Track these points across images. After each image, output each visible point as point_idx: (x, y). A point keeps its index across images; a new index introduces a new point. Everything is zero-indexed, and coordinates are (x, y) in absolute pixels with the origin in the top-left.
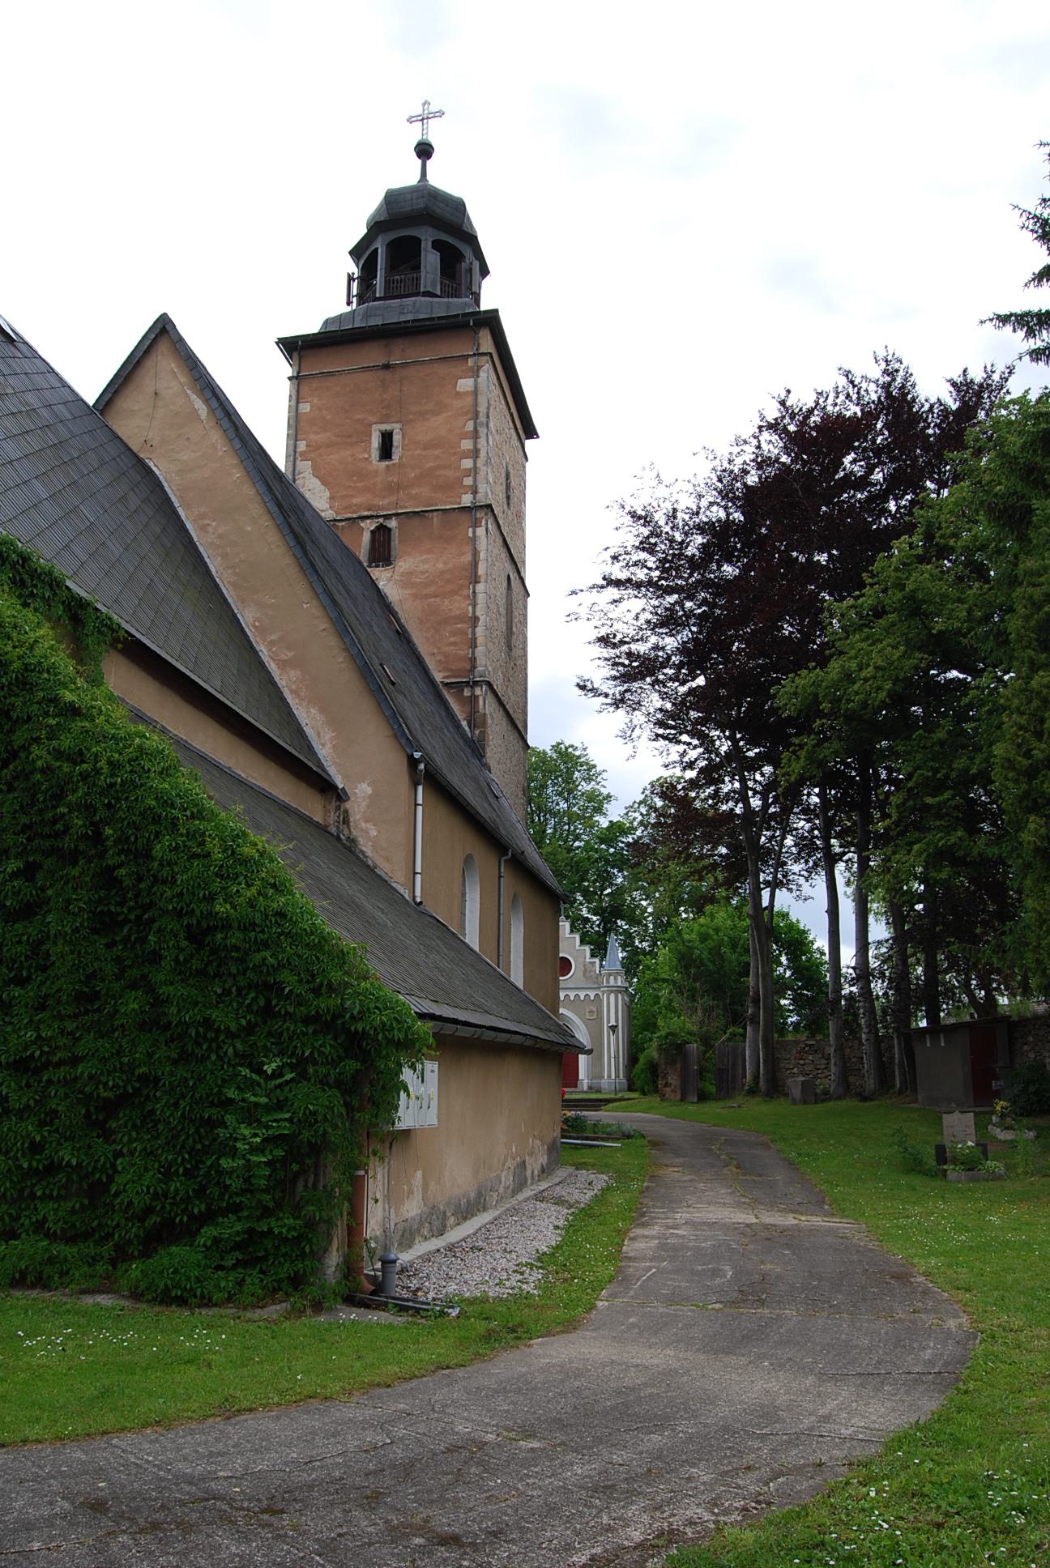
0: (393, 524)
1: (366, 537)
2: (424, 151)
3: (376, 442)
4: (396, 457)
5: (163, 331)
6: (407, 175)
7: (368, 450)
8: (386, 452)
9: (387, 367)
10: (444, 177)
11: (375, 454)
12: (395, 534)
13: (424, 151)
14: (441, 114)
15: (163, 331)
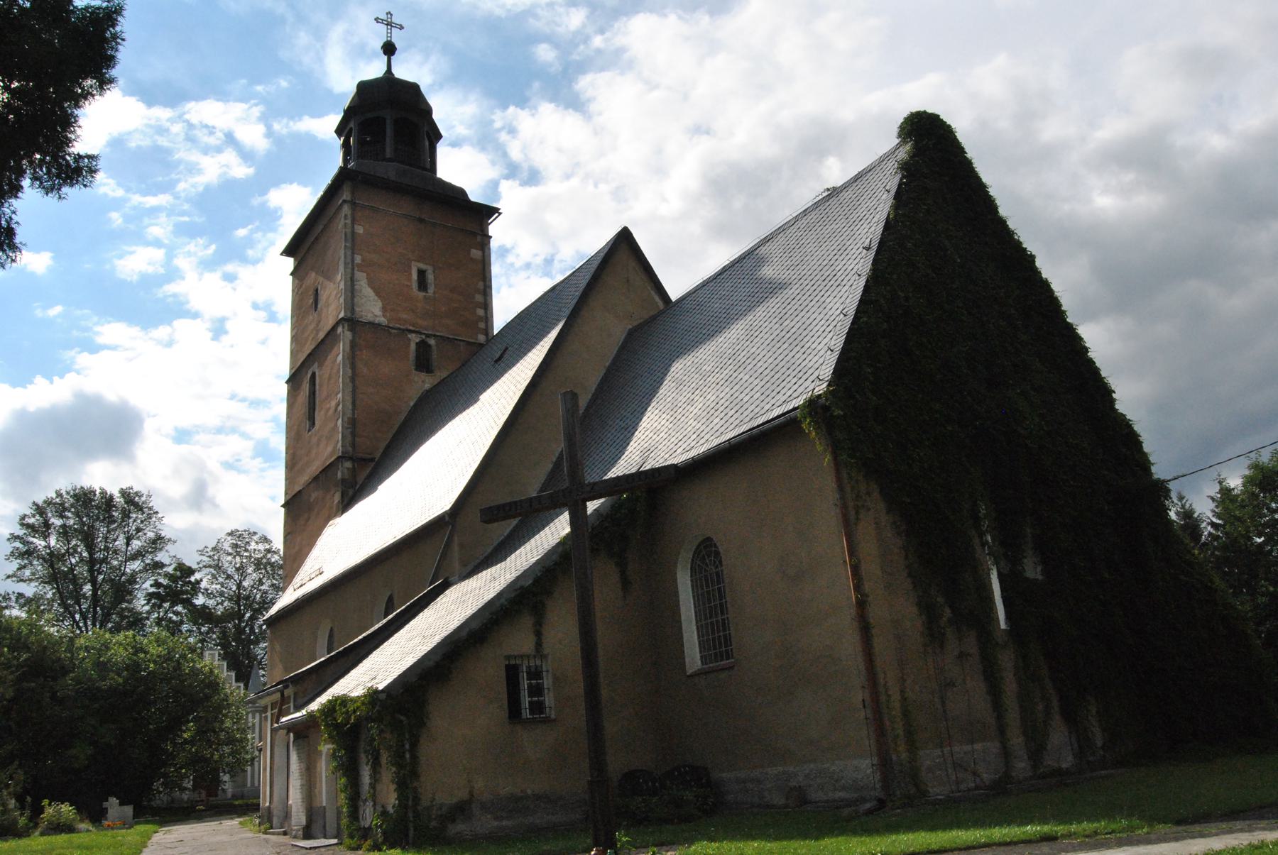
0: (432, 342)
1: (413, 347)
2: (389, 49)
3: (415, 276)
4: (431, 290)
5: (625, 240)
6: (375, 70)
7: (410, 279)
8: (422, 284)
9: (421, 220)
10: (402, 72)
11: (415, 285)
12: (434, 348)
13: (389, 49)
14: (401, 28)
15: (625, 240)
